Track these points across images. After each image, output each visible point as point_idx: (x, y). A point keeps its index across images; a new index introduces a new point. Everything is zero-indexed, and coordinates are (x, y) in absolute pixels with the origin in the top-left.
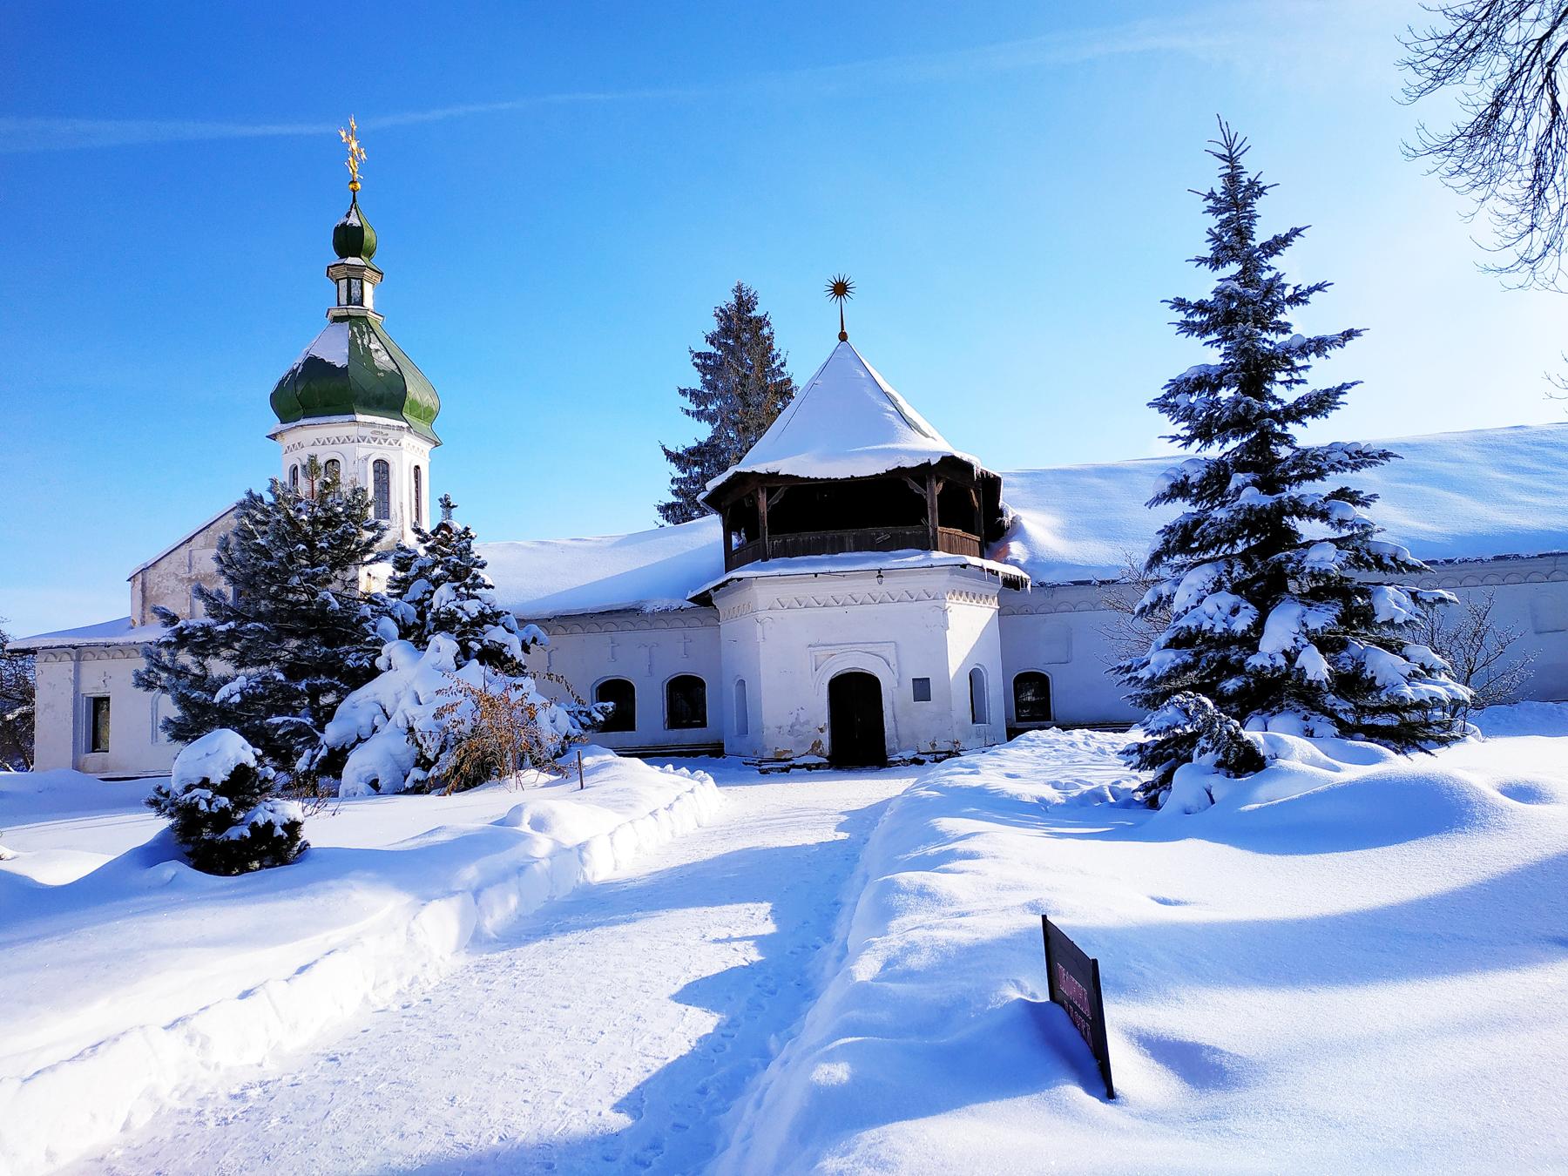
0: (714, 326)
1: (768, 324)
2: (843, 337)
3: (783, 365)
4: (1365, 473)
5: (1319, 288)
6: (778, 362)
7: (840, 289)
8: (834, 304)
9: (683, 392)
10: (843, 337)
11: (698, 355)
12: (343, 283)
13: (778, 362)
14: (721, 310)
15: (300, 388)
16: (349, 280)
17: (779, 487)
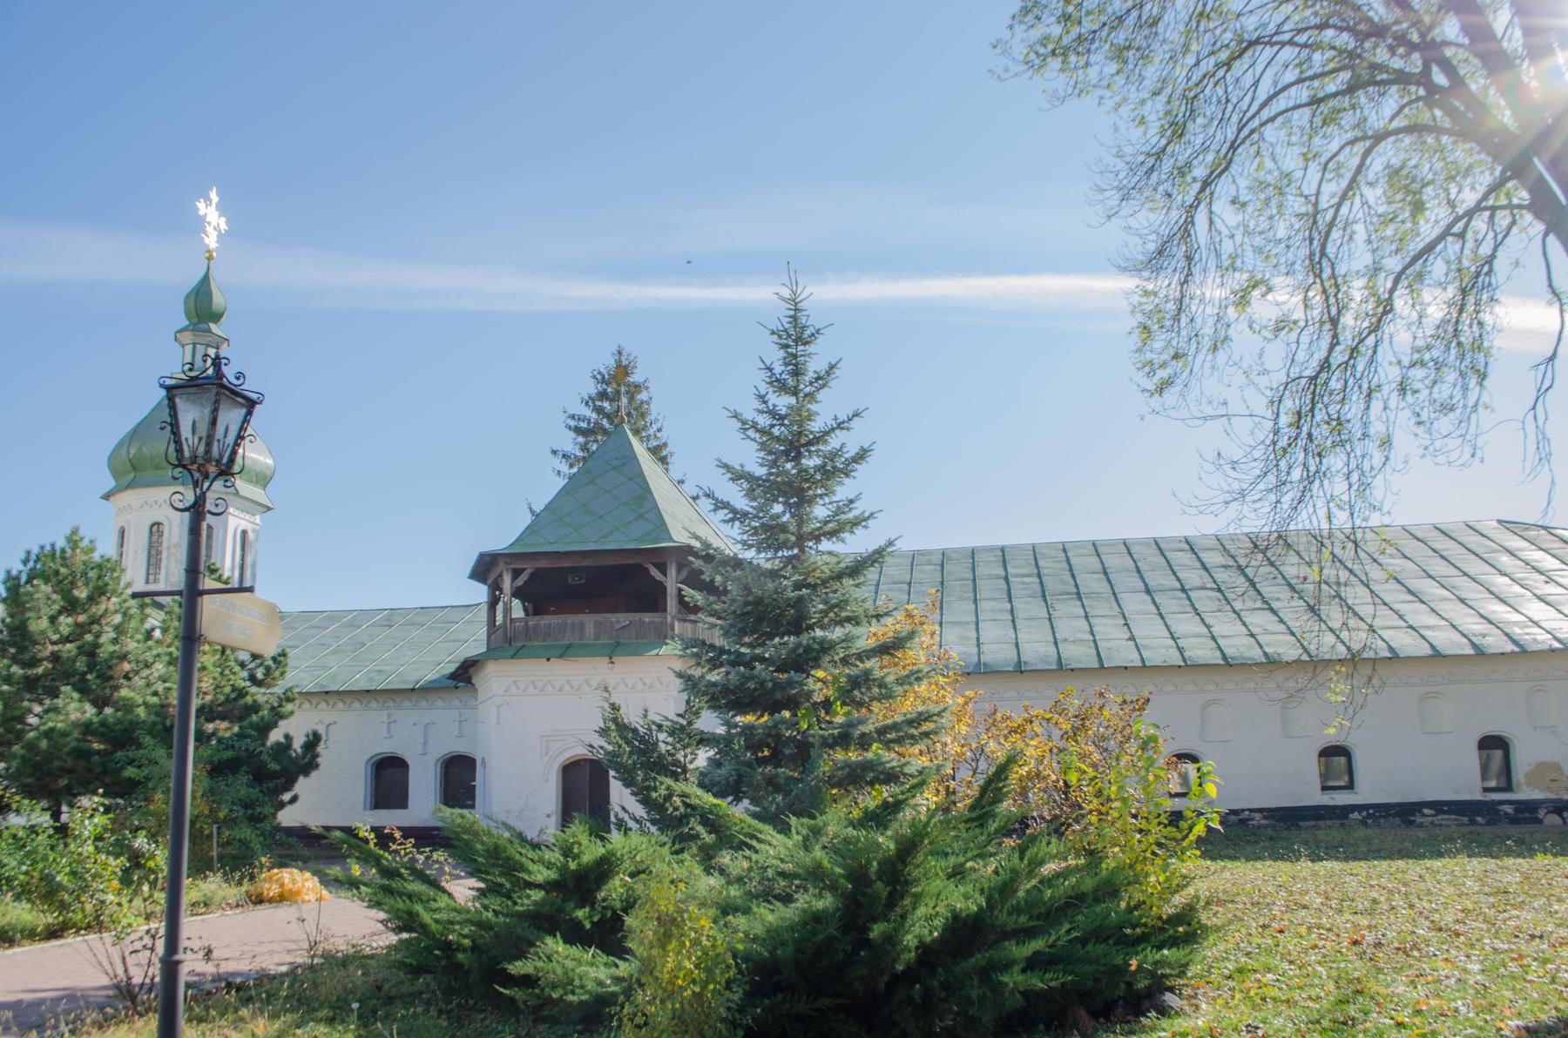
0: (592, 389)
1: (647, 388)
3: (659, 430)
4: (1224, 563)
5: (856, 415)
6: (655, 427)
9: (554, 452)
11: (573, 417)
12: (189, 348)
13: (655, 427)
14: (600, 373)
15: (133, 451)
16: (194, 344)
17: (524, 570)
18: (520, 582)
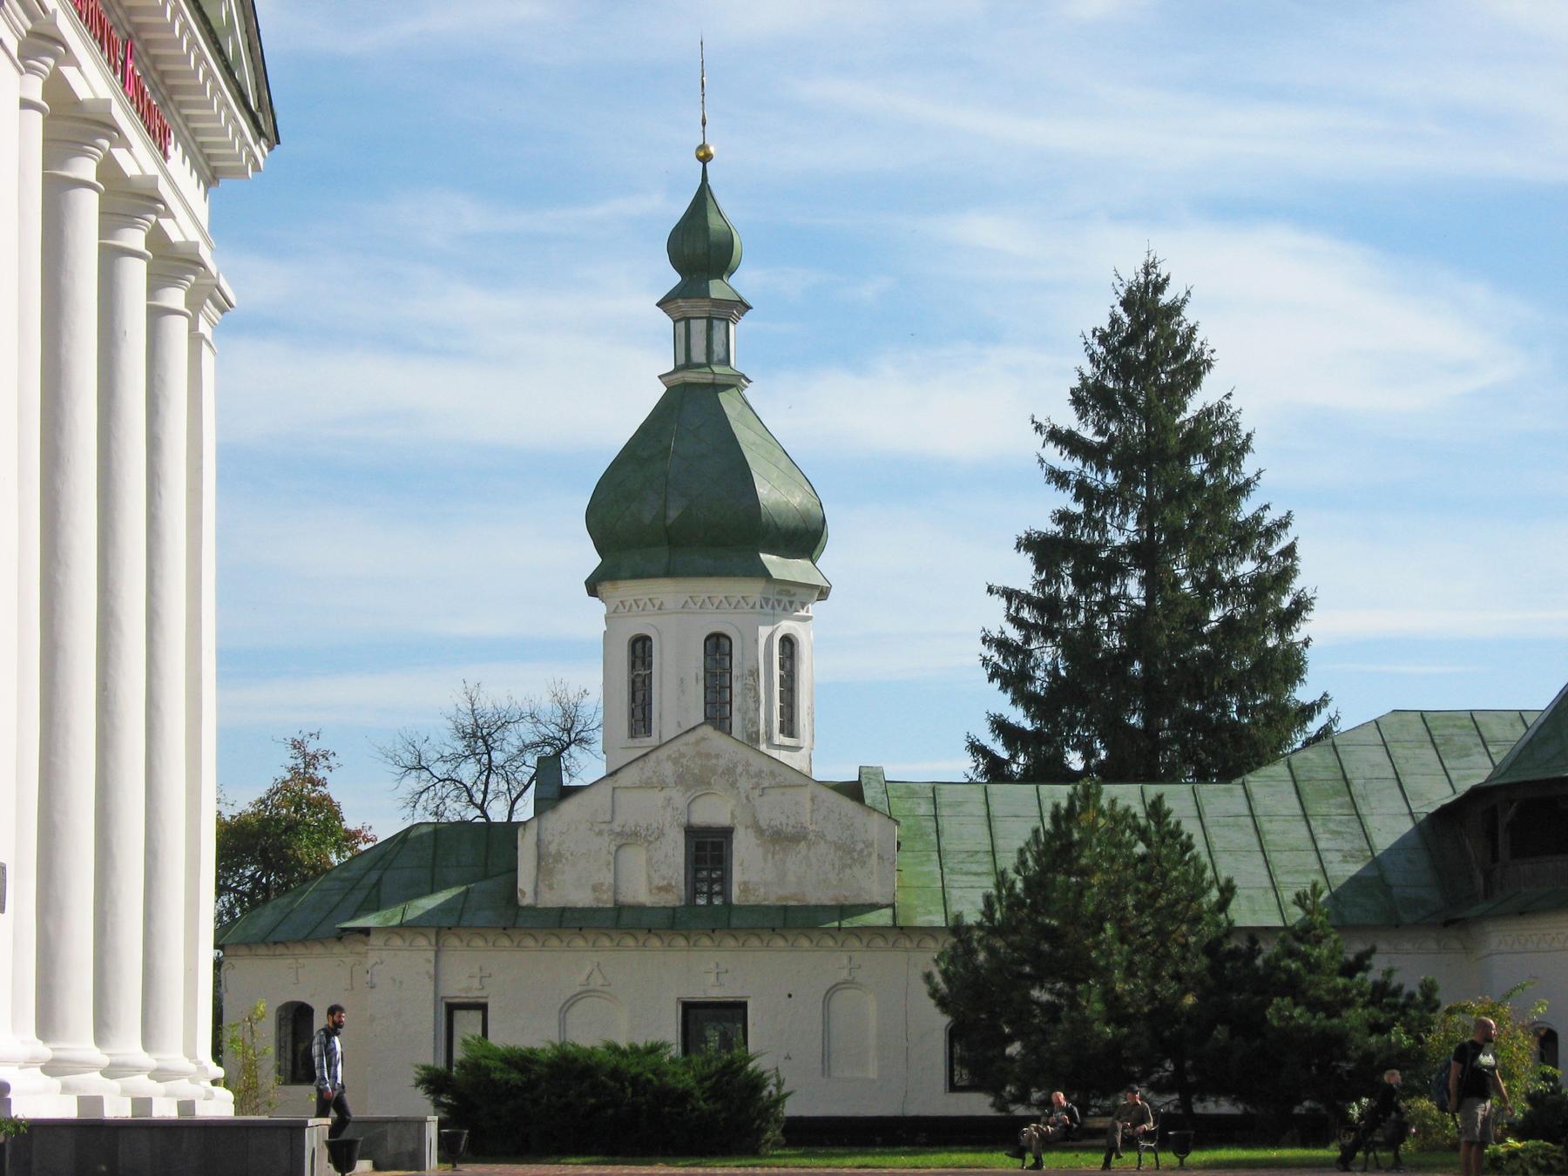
12: (698, 327)
16: (710, 320)
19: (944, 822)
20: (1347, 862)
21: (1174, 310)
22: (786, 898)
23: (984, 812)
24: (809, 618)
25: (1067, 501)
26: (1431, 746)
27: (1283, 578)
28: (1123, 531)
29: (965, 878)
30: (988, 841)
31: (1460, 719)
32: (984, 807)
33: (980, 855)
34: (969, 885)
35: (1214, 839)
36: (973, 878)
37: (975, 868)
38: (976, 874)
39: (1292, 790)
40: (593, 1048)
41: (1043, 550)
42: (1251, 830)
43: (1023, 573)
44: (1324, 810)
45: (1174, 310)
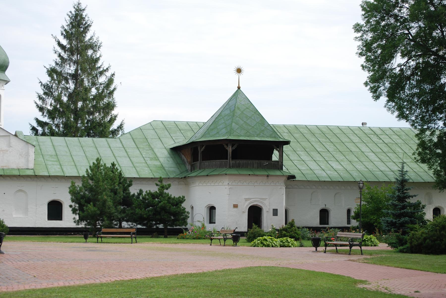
2: (239, 88)
7: (239, 71)
8: (236, 75)
10: (239, 88)
18: (234, 148)
19: (42, 147)
20: (152, 161)
21: (365, 59)
22: (3, 167)
23: (52, 144)
24: (4, 90)
25: (59, 60)
26: (166, 130)
27: (391, 96)
28: (70, 69)
29: (51, 162)
30: (55, 153)
31: (172, 123)
32: (51, 143)
33: (53, 156)
34: (52, 164)
35: (115, 153)
36: (53, 162)
37: (53, 159)
38: (53, 161)
39: (133, 141)
40: (70, 192)
41: (51, 72)
42: (124, 151)
43: (46, 79)
44: (142, 147)
45: (365, 59)
